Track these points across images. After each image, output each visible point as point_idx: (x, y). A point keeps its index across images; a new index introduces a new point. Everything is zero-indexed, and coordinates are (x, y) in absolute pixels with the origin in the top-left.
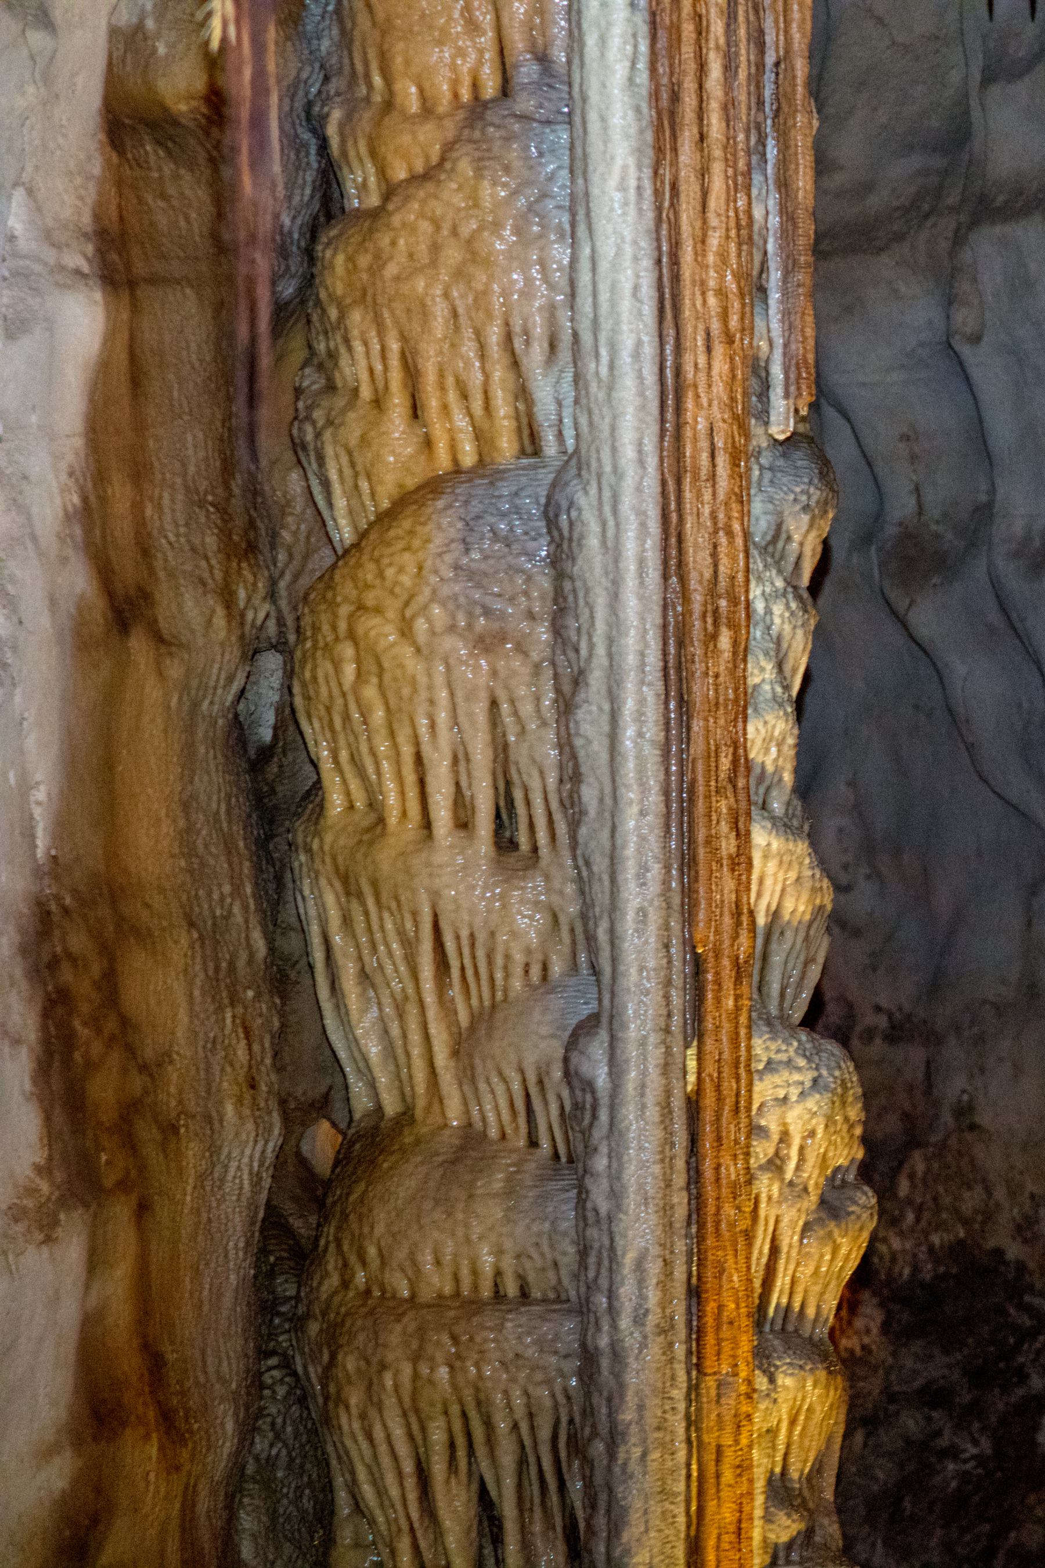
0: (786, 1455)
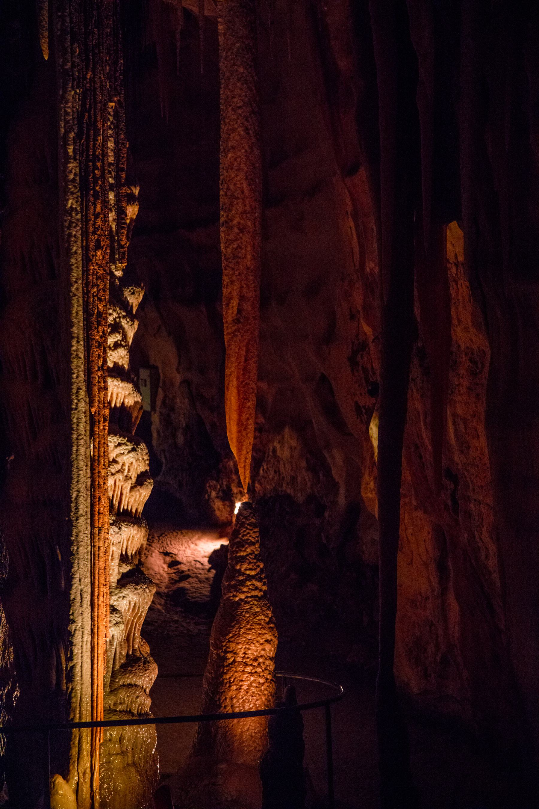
0: (126, 549)
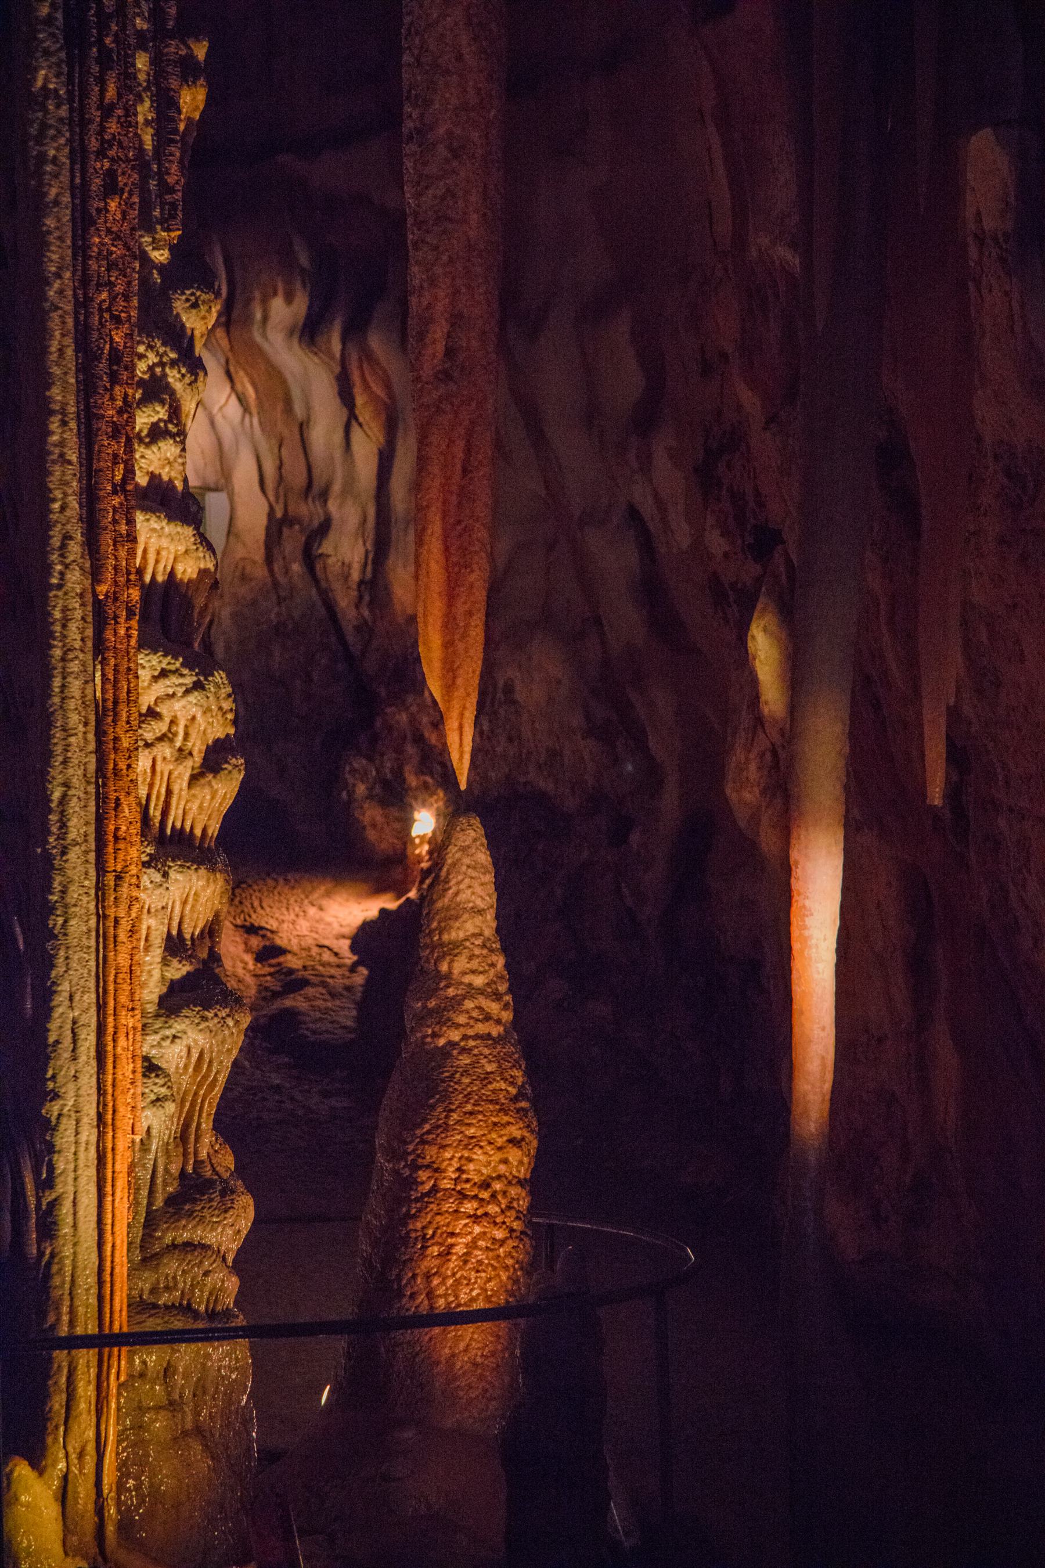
0: (180, 924)
